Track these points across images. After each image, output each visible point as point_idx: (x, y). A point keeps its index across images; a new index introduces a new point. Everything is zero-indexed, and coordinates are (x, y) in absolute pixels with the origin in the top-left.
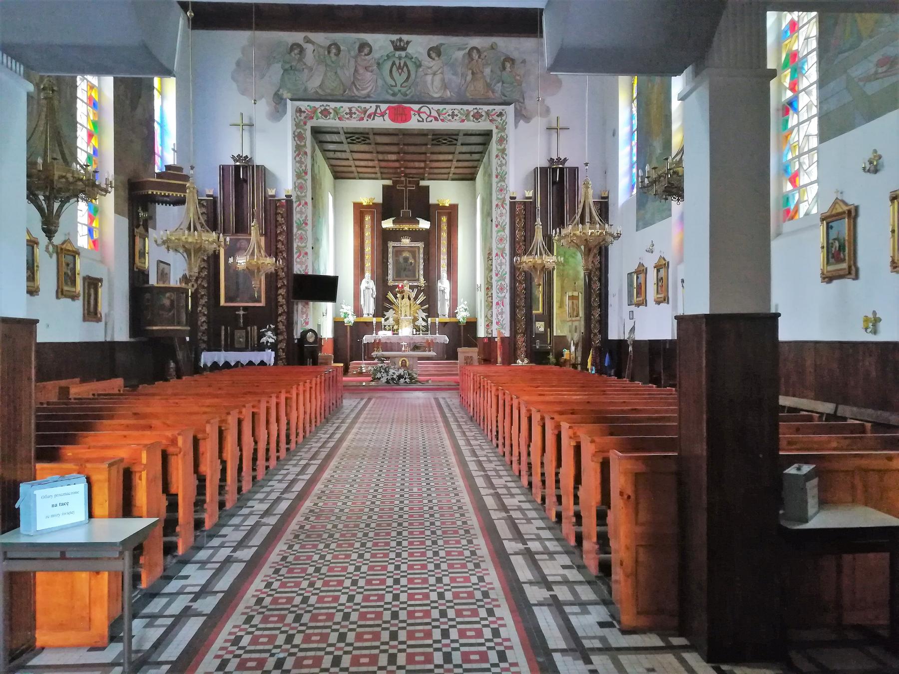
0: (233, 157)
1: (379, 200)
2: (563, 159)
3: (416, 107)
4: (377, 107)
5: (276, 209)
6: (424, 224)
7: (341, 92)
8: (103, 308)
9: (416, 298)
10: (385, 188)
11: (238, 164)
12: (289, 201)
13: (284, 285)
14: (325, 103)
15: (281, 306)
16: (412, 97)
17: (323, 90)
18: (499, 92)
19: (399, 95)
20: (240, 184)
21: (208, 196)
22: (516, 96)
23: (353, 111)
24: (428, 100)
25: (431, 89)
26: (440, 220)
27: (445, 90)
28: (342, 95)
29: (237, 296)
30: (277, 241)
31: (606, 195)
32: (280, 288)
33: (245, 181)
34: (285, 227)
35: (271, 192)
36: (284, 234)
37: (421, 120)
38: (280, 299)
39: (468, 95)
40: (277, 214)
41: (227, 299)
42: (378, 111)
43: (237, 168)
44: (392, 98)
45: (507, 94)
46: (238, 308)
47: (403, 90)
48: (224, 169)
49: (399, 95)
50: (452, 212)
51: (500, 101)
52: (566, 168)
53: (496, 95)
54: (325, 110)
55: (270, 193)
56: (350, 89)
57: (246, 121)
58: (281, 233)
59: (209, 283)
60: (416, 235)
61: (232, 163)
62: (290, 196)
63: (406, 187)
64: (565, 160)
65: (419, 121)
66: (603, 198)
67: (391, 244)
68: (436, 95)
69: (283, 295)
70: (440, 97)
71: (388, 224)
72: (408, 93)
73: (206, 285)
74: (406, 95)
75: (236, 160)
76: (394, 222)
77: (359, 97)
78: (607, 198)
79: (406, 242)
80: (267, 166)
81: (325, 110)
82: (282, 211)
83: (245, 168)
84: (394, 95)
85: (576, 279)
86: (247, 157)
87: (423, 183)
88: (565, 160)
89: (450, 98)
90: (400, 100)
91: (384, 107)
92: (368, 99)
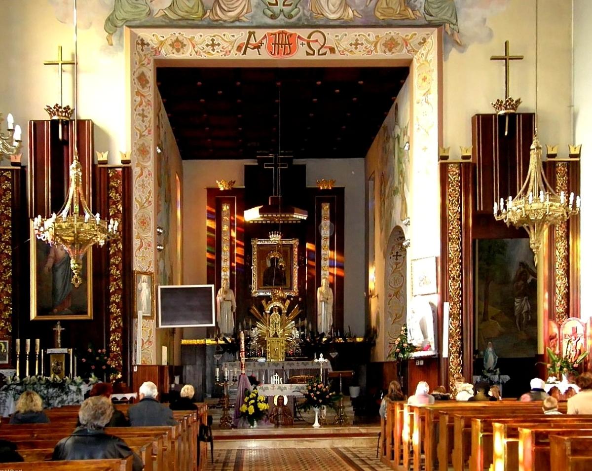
0: (49, 109)
1: (240, 185)
2: (515, 100)
3: (304, 33)
4: (250, 34)
5: (109, 182)
6: (300, 216)
7: (200, 13)
8: (454, 462)
9: (290, 310)
10: (247, 168)
11: (55, 118)
12: (127, 171)
13: (119, 288)
14: (176, 31)
15: (115, 318)
16: (299, 19)
17: (175, 13)
18: (422, 11)
19: (282, 17)
20: (59, 149)
21: (14, 164)
22: (444, 15)
23: (216, 42)
24: (321, 23)
25: (327, 9)
26: (320, 209)
27: (345, 10)
28: (201, 19)
29: (54, 306)
30: (109, 188)
31: (577, 152)
32: (114, 293)
33: (65, 142)
34: (120, 207)
35: (101, 157)
36: (120, 254)
37: (311, 52)
38: (113, 309)
39: (378, 14)
40: (109, 188)
41: (40, 312)
42: (252, 41)
43: (54, 124)
44: (270, 22)
45: (432, 11)
46: (54, 323)
47: (287, 9)
48: (37, 125)
49: (282, 17)
50: (337, 197)
51: (424, 22)
52: (519, 114)
53: (418, 14)
54: (177, 40)
55: (100, 159)
56: (212, 10)
57: (67, 58)
58: (114, 254)
59: (13, 287)
60: (288, 230)
61: (46, 117)
62: (128, 162)
63: (276, 166)
64: (518, 102)
65: (308, 54)
66: (571, 156)
67: (257, 242)
68: (332, 16)
69: (117, 304)
70: (339, 19)
71: (252, 215)
72: (293, 13)
73: (10, 292)
74: (291, 17)
75: (52, 113)
76: (261, 211)
77: (225, 21)
78: (578, 156)
79: (275, 238)
80: (97, 122)
81: (177, 40)
82: (117, 183)
83: (66, 124)
84: (273, 17)
85: (209, 357)
86: (68, 108)
87: (298, 162)
88: (518, 102)
89: (351, 20)
90: (282, 23)
91: (260, 34)
92: (237, 24)
